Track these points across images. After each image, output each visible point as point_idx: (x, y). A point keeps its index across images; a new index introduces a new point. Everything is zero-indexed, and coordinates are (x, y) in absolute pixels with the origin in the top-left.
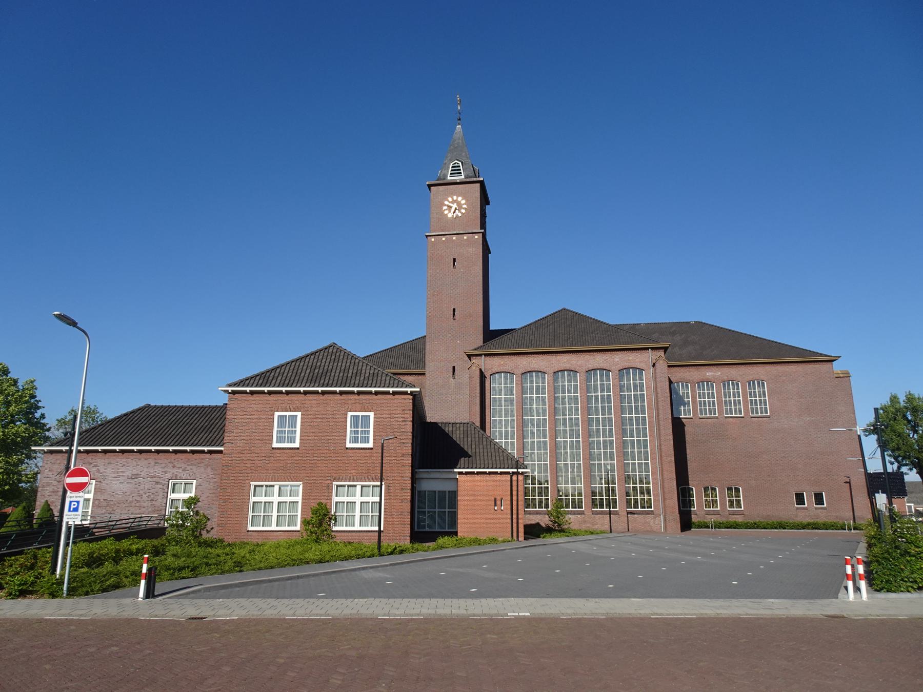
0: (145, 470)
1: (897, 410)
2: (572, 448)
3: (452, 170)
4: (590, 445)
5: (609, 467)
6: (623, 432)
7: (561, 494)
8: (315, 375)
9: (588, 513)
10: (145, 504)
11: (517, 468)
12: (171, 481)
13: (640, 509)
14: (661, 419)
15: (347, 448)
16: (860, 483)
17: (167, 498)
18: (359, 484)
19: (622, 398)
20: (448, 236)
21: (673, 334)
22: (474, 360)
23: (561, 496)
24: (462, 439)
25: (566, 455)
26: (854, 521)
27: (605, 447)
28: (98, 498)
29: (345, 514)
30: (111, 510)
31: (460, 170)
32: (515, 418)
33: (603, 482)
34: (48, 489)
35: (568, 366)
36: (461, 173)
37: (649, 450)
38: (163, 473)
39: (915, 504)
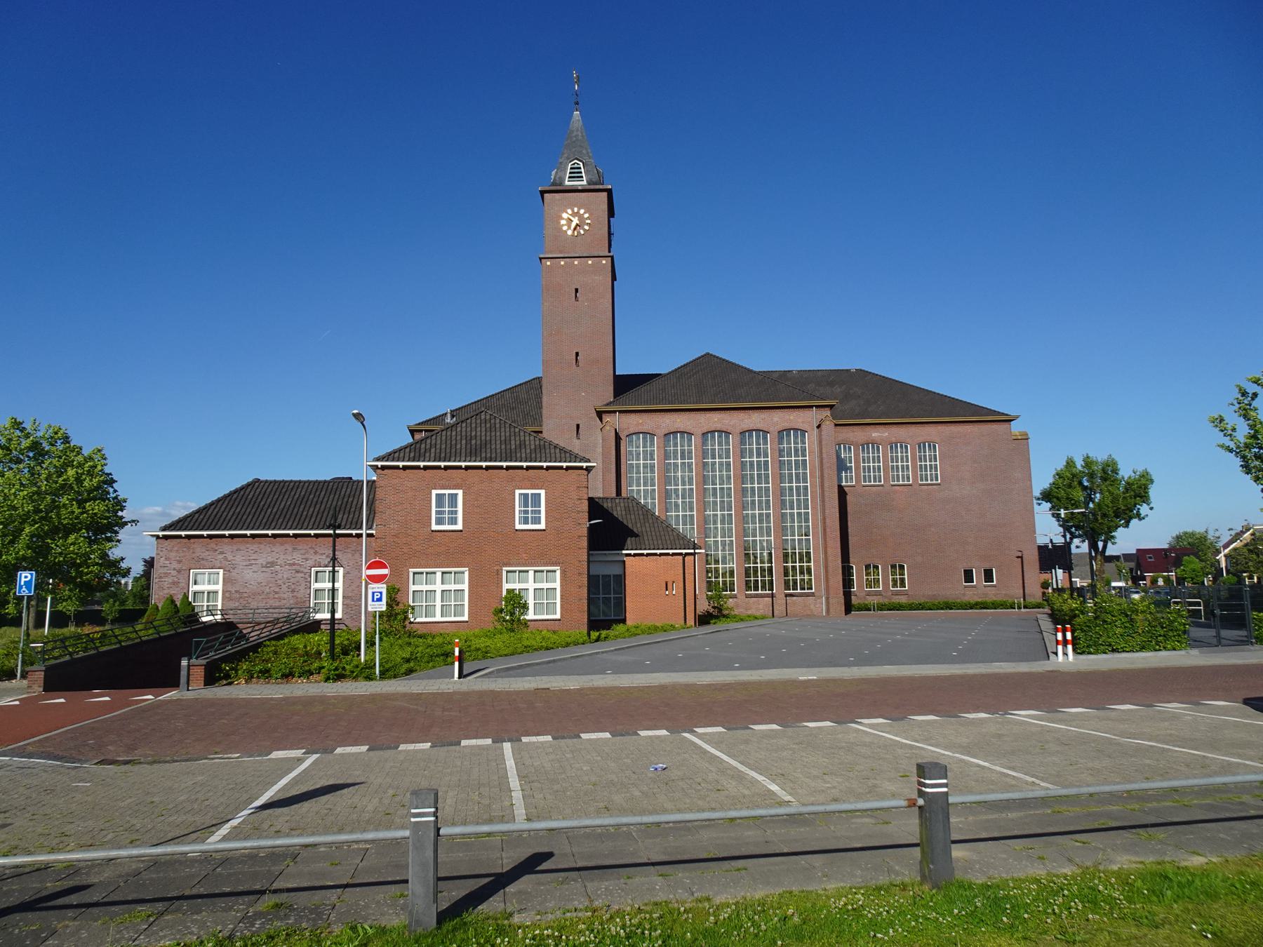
0: (282, 557)
1: (1074, 475)
2: (723, 522)
3: (570, 173)
4: (744, 519)
5: (765, 544)
6: (781, 504)
7: (710, 575)
8: (473, 447)
9: (741, 597)
10: (285, 596)
11: (694, 549)
12: (313, 569)
13: (799, 591)
14: (826, 489)
15: (517, 530)
16: (1032, 557)
17: (310, 588)
18: (531, 569)
19: (781, 463)
20: (568, 260)
21: (831, 384)
22: (607, 418)
23: (710, 578)
24: (624, 517)
25: (715, 531)
26: (1024, 600)
27: (761, 521)
28: (229, 589)
29: (424, 604)
30: (245, 602)
31: (581, 173)
32: (656, 488)
33: (759, 561)
34: (166, 580)
35: (719, 426)
36: (582, 177)
37: (810, 524)
38: (304, 560)
39: (1081, 579)
